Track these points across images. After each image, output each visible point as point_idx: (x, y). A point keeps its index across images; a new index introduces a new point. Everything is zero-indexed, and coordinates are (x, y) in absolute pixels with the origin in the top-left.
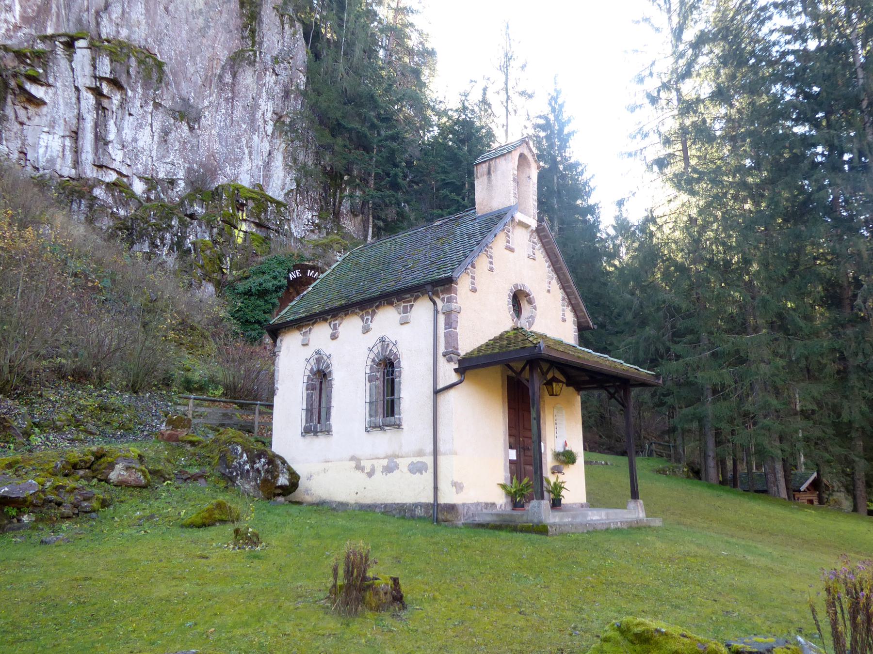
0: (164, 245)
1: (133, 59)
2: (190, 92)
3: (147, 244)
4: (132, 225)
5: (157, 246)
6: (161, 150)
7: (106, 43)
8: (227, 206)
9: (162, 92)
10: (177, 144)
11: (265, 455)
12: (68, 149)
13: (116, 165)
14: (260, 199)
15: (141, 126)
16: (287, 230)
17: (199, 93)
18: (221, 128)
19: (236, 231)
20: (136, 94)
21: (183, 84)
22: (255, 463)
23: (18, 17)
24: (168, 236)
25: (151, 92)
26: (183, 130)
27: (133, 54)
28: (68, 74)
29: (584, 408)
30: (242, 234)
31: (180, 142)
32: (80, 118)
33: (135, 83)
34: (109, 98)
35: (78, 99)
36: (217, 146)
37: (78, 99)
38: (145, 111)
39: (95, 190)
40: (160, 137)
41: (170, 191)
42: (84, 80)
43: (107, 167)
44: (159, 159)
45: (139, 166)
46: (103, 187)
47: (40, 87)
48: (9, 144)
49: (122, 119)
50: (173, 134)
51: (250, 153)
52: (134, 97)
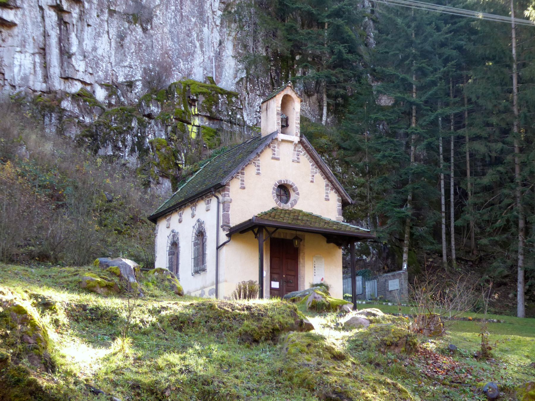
0: (126, 147)
3: (110, 148)
4: (96, 131)
8: (179, 104)
12: (38, 65)
15: (99, 35)
16: (239, 119)
18: (172, 26)
19: (190, 127)
24: (129, 137)
26: (137, 33)
30: (195, 129)
31: (135, 44)
35: (43, 17)
36: (169, 43)
37: (43, 17)
38: (102, 20)
39: (62, 103)
41: (129, 94)
43: (72, 79)
44: (118, 64)
45: (100, 73)
46: (70, 99)
47: (10, 11)
49: (82, 30)
51: (202, 46)
52: (91, 8)
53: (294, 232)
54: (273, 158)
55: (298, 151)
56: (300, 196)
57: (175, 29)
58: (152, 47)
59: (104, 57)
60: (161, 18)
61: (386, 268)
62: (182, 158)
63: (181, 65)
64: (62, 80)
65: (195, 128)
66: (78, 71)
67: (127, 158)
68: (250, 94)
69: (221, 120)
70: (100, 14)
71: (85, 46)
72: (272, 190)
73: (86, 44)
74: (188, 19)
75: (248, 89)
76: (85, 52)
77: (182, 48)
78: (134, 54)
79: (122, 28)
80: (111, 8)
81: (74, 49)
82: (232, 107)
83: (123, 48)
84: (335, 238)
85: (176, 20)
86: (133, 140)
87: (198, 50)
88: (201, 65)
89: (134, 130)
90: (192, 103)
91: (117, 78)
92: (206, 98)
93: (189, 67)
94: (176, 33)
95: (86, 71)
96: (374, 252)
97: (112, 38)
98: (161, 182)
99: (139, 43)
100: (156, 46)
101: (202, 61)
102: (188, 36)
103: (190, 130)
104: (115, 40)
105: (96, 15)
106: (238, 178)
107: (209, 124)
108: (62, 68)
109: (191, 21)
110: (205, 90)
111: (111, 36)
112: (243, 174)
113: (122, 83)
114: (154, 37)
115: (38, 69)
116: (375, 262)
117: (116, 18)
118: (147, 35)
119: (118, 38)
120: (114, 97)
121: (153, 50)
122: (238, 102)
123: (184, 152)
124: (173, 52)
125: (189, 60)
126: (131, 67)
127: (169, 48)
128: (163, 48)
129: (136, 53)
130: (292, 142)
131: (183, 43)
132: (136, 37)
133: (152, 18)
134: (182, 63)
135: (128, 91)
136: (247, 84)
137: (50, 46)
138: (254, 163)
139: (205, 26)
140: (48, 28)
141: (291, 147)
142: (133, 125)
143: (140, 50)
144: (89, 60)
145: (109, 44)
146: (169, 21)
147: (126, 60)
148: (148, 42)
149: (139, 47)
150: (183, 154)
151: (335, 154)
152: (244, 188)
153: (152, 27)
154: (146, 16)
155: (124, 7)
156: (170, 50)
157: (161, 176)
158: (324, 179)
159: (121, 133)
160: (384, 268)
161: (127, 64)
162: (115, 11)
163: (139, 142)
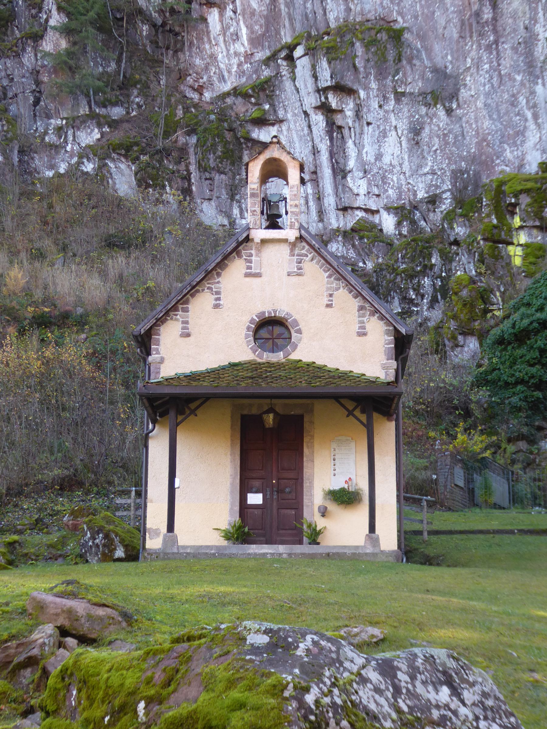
0: (423, 296)
1: (358, 44)
2: (446, 55)
3: (396, 301)
4: (377, 280)
5: (411, 301)
6: (415, 159)
7: (326, 38)
8: (488, 216)
9: (405, 75)
10: (436, 140)
11: (102, 530)
12: (310, 197)
13: (360, 202)
15: (384, 134)
17: (458, 50)
18: (487, 95)
19: (511, 248)
20: (369, 93)
21: (437, 48)
22: (95, 539)
23: (246, 43)
24: (427, 281)
25: (389, 82)
26: (439, 119)
27: (357, 37)
28: (294, 98)
30: (519, 251)
31: (438, 136)
32: (315, 151)
33: (366, 77)
35: (309, 126)
36: (487, 123)
37: (309, 126)
38: (386, 112)
40: (409, 140)
41: (431, 215)
42: (311, 100)
43: (352, 208)
44: (415, 172)
45: (390, 192)
46: (340, 239)
49: (362, 133)
50: (427, 130)
51: (536, 117)
52: (368, 97)
53: (268, 401)
54: (247, 275)
55: (298, 255)
56: (304, 335)
57: (492, 99)
58: (463, 135)
59: (394, 167)
60: (473, 87)
62: (498, 300)
63: (508, 154)
64: (341, 213)
65: (519, 248)
66: (358, 195)
67: (425, 313)
70: (382, 103)
71: (365, 155)
72: (244, 331)
73: (366, 152)
74: (510, 79)
76: (365, 164)
77: (506, 127)
78: (438, 152)
80: (399, 90)
81: (352, 164)
84: (368, 403)
85: (493, 85)
86: (434, 285)
87: (531, 125)
88: (538, 147)
89: (436, 269)
90: (512, 209)
91: (415, 194)
92: (532, 197)
93: (520, 154)
94: (494, 105)
95: (369, 193)
97: (402, 134)
98: (461, 343)
99: (444, 134)
101: (538, 140)
102: (513, 104)
103: (512, 253)
104: (407, 137)
105: (377, 107)
106: (177, 320)
108: (337, 196)
109: (515, 80)
110: (529, 185)
111: (400, 132)
112: (186, 310)
113: (421, 201)
114: (464, 119)
115: (311, 203)
117: (407, 104)
118: (454, 119)
119: (411, 133)
120: (405, 223)
121: (465, 139)
123: (499, 290)
124: (493, 136)
125: (518, 142)
126: (434, 173)
127: (487, 131)
128: (478, 134)
129: (441, 151)
130: (285, 241)
133: (459, 90)
134: (508, 151)
135: (429, 210)
137: (321, 167)
138: (208, 288)
139: (537, 83)
140: (317, 141)
141: (285, 249)
142: (433, 261)
143: (447, 143)
145: (399, 145)
146: (482, 89)
147: (427, 164)
148: (456, 128)
149: (444, 139)
150: (498, 294)
152: (188, 335)
153: (458, 105)
154: (450, 89)
155: (420, 84)
156: (489, 134)
157: (460, 334)
158: (356, 297)
159: (412, 277)
161: (426, 170)
162: (403, 94)
163: (443, 286)
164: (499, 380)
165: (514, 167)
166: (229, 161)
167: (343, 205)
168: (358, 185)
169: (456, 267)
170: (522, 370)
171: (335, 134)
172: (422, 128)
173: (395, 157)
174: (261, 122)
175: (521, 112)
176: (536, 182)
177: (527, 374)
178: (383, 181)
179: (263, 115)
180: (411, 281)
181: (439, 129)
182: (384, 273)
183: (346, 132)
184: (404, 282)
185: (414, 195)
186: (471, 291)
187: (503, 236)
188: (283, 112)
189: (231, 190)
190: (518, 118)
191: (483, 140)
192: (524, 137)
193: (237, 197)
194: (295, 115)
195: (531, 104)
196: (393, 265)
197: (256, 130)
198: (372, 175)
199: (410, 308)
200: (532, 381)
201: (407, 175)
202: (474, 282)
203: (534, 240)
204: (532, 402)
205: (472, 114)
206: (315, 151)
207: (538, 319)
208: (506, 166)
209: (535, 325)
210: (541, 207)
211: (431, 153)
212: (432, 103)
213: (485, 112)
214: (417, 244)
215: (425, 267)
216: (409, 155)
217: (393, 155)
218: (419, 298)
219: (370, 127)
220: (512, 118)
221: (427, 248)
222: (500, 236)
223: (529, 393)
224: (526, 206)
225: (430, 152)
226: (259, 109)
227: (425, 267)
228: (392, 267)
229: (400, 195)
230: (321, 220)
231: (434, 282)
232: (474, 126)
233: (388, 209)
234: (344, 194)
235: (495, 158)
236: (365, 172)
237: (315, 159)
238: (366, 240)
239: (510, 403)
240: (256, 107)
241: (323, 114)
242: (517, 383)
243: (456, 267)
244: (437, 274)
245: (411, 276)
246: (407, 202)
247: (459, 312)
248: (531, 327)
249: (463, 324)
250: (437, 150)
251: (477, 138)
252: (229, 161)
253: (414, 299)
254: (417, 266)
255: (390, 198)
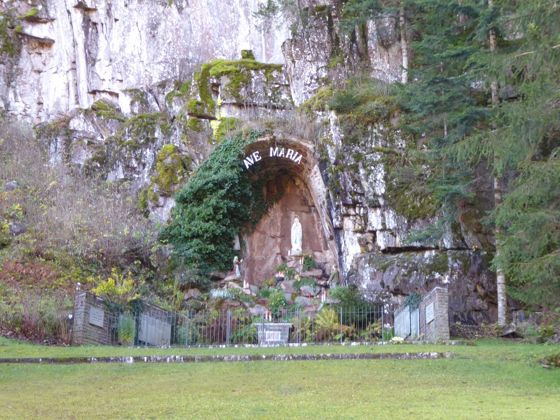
0: (144, 165)
3: (121, 169)
14: (245, 69)
16: (284, 101)
29: (300, 221)
31: (172, 31)
32: (75, 44)
34: (95, 10)
35: (71, 23)
37: (71, 23)
38: (131, 10)
39: (71, 123)
40: (147, 34)
43: (100, 92)
46: (82, 116)
47: (44, 25)
48: (25, 99)
58: (191, 30)
61: (479, 289)
64: (92, 95)
66: (104, 80)
68: (297, 61)
69: (255, 105)
70: (127, 2)
73: (113, 45)
75: (293, 55)
77: (223, 22)
78: (172, 44)
79: (155, 14)
82: (273, 86)
83: (155, 39)
87: (243, 19)
88: (248, 39)
89: (158, 142)
93: (234, 45)
95: (113, 78)
96: (455, 265)
97: (142, 29)
98: (162, 204)
99: (176, 29)
100: (194, 27)
104: (145, 31)
107: (240, 115)
110: (230, 68)
116: (459, 281)
119: (148, 27)
120: (137, 103)
122: (282, 77)
127: (209, 26)
128: (202, 28)
129: (174, 43)
131: (224, 14)
132: (172, 22)
135: (159, 93)
136: (291, 49)
142: (156, 135)
144: (116, 64)
148: (186, 24)
149: (176, 34)
151: (395, 122)
156: (210, 28)
157: (162, 196)
160: (476, 290)
161: (161, 59)
164: (180, 235)
165: (229, 56)
166: (8, 54)
167: (92, 88)
168: (103, 69)
169: (173, 140)
170: (199, 225)
171: (90, 29)
172: (158, 24)
173: (136, 49)
174: (34, 20)
175: (235, 10)
176: (236, 66)
177: (201, 228)
178: (125, 68)
179: (35, 14)
180: (134, 152)
181: (173, 25)
182: (113, 144)
183: (99, 27)
184: (128, 152)
185: (150, 80)
186: (173, 159)
187: (206, 111)
188: (54, 12)
189: (8, 78)
190: (233, 14)
191: (206, 34)
192: (238, 30)
193: (13, 84)
194: (62, 14)
195: (243, 3)
196: (120, 138)
197: (30, 26)
198: (116, 64)
199: (132, 175)
200: (206, 235)
201: (145, 64)
202: (179, 151)
203: (233, 116)
204: (206, 253)
205: (199, 12)
206: (75, 44)
207: (214, 180)
208: (224, 55)
209: (211, 185)
210: (238, 87)
211: (166, 45)
212: (168, 3)
213: (207, 10)
214: (143, 121)
215: (148, 140)
216: (147, 47)
217: (134, 47)
218: (141, 166)
219: (117, 22)
220: (228, 15)
221: (151, 124)
222: (203, 111)
223: (203, 246)
224: (226, 86)
225: (164, 44)
226: (34, 10)
227: (148, 140)
228: (119, 140)
229: (139, 81)
230: (77, 103)
231: (155, 154)
232: (199, 22)
233: (125, 91)
234: (93, 79)
235: (215, 49)
236: (111, 61)
237: (74, 51)
238: (102, 117)
239: (185, 255)
240: (33, 8)
241: (81, 12)
242: (193, 237)
243: (173, 140)
244: (158, 146)
245: (135, 147)
246: (144, 87)
247: (161, 176)
248: (206, 187)
249: (164, 187)
250: (170, 42)
251: (202, 32)
252: (8, 54)
253: (136, 168)
254: (141, 139)
255: (131, 83)
